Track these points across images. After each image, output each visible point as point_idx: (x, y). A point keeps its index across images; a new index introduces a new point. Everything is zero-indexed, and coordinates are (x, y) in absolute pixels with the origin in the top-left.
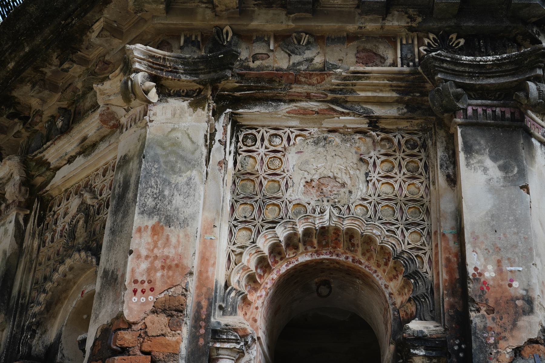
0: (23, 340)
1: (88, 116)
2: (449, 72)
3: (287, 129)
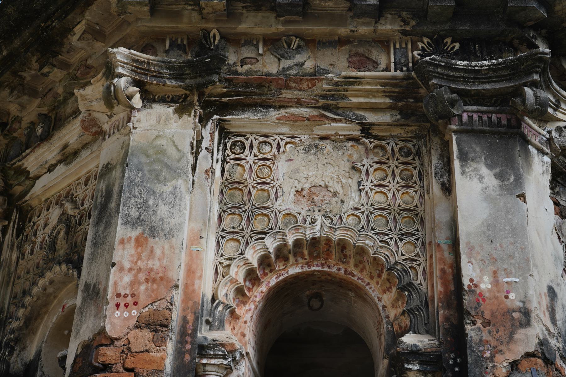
1: (69, 123)
3: (276, 137)
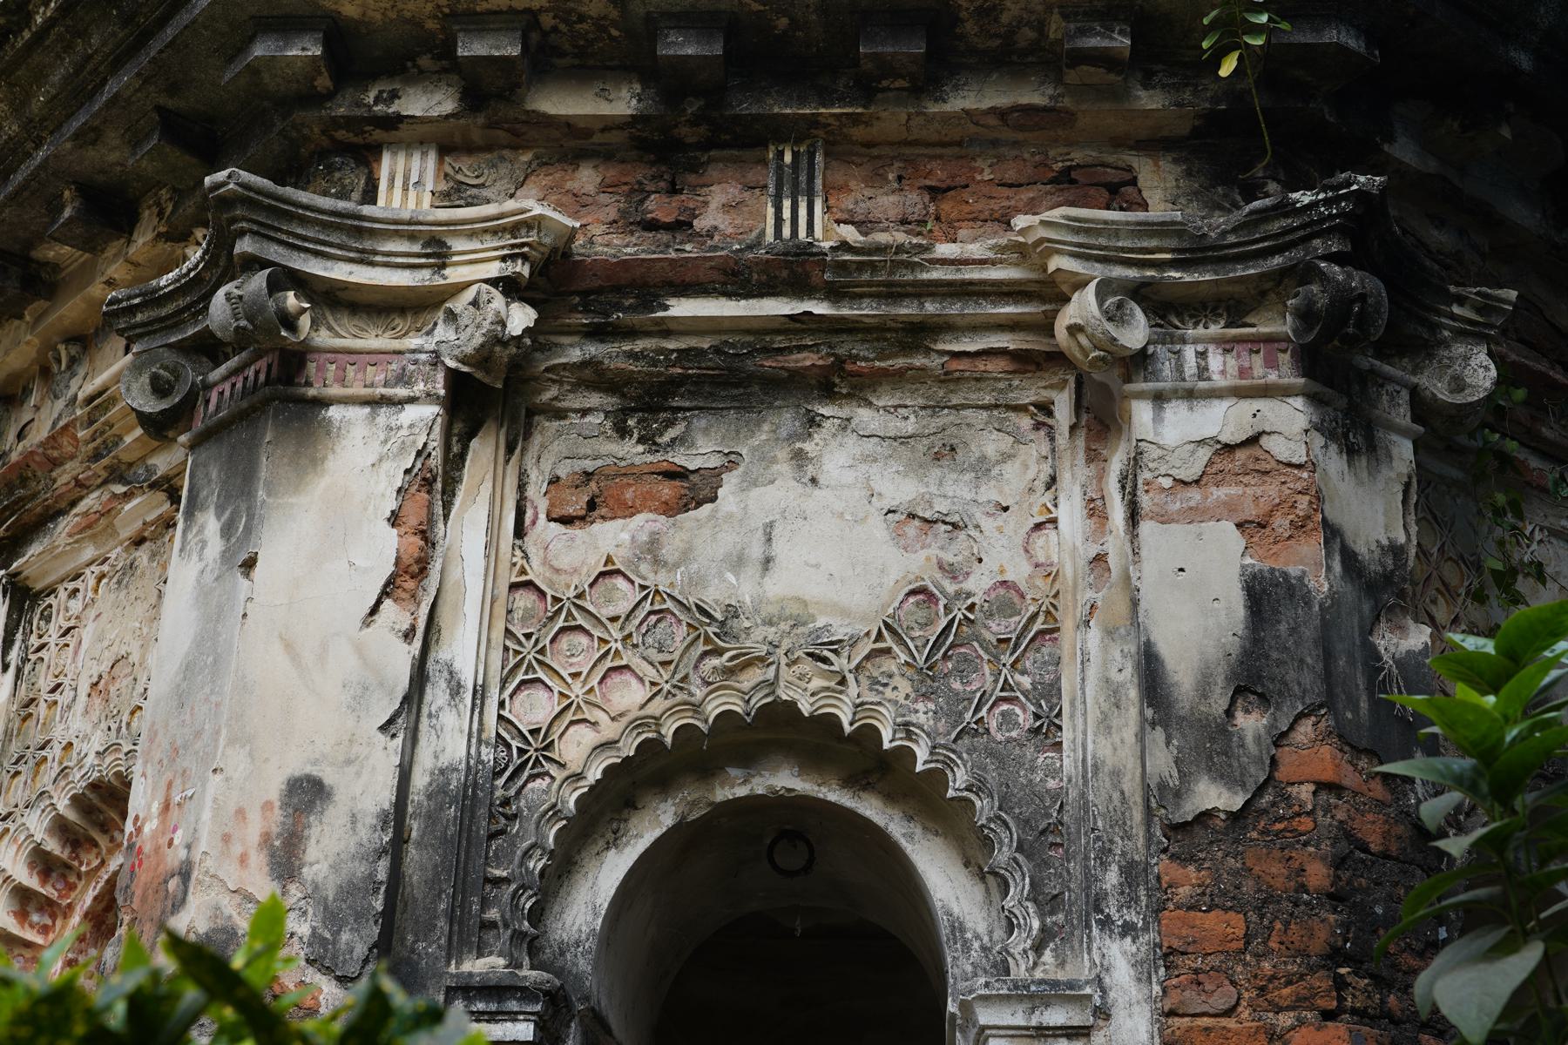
2: (156, 326)
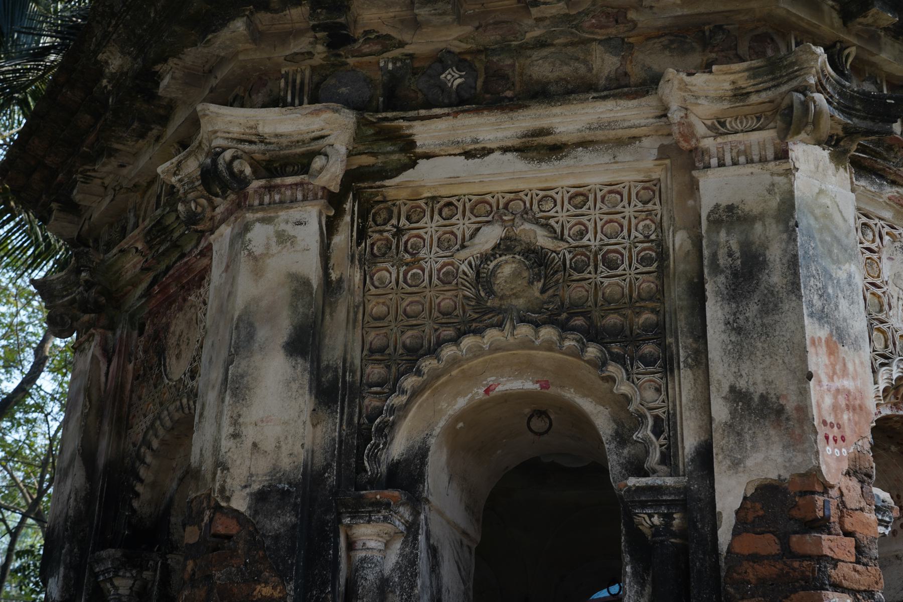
0: (370, 450)
3: (877, 221)
